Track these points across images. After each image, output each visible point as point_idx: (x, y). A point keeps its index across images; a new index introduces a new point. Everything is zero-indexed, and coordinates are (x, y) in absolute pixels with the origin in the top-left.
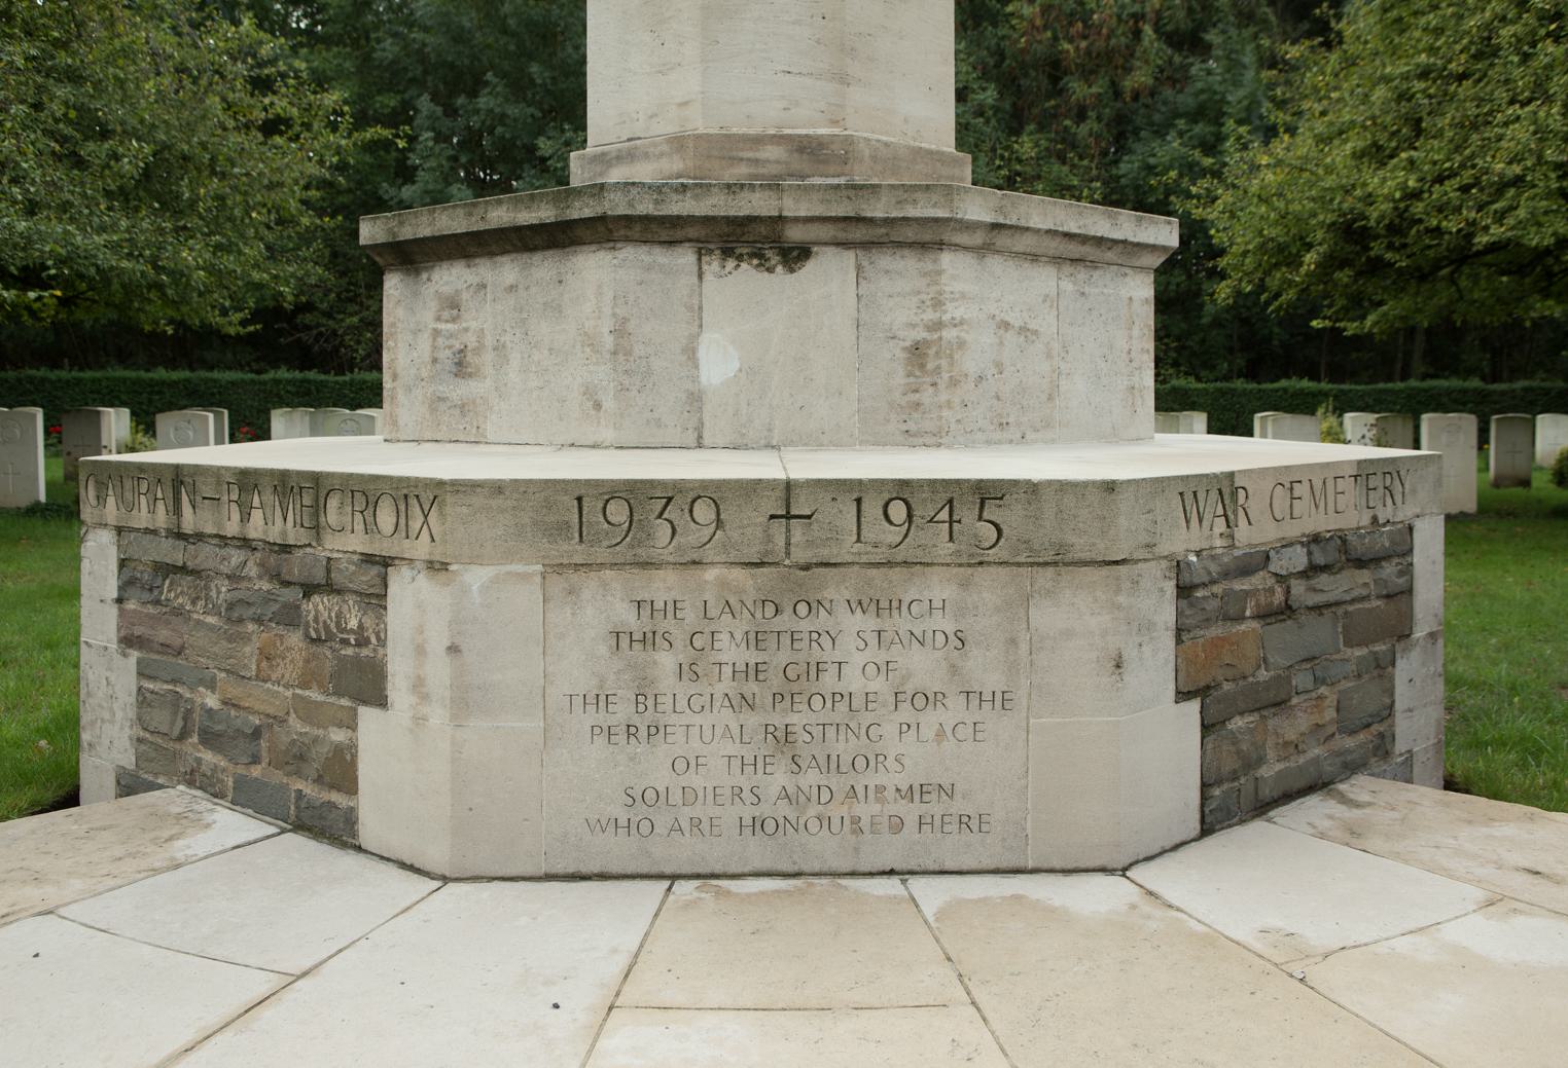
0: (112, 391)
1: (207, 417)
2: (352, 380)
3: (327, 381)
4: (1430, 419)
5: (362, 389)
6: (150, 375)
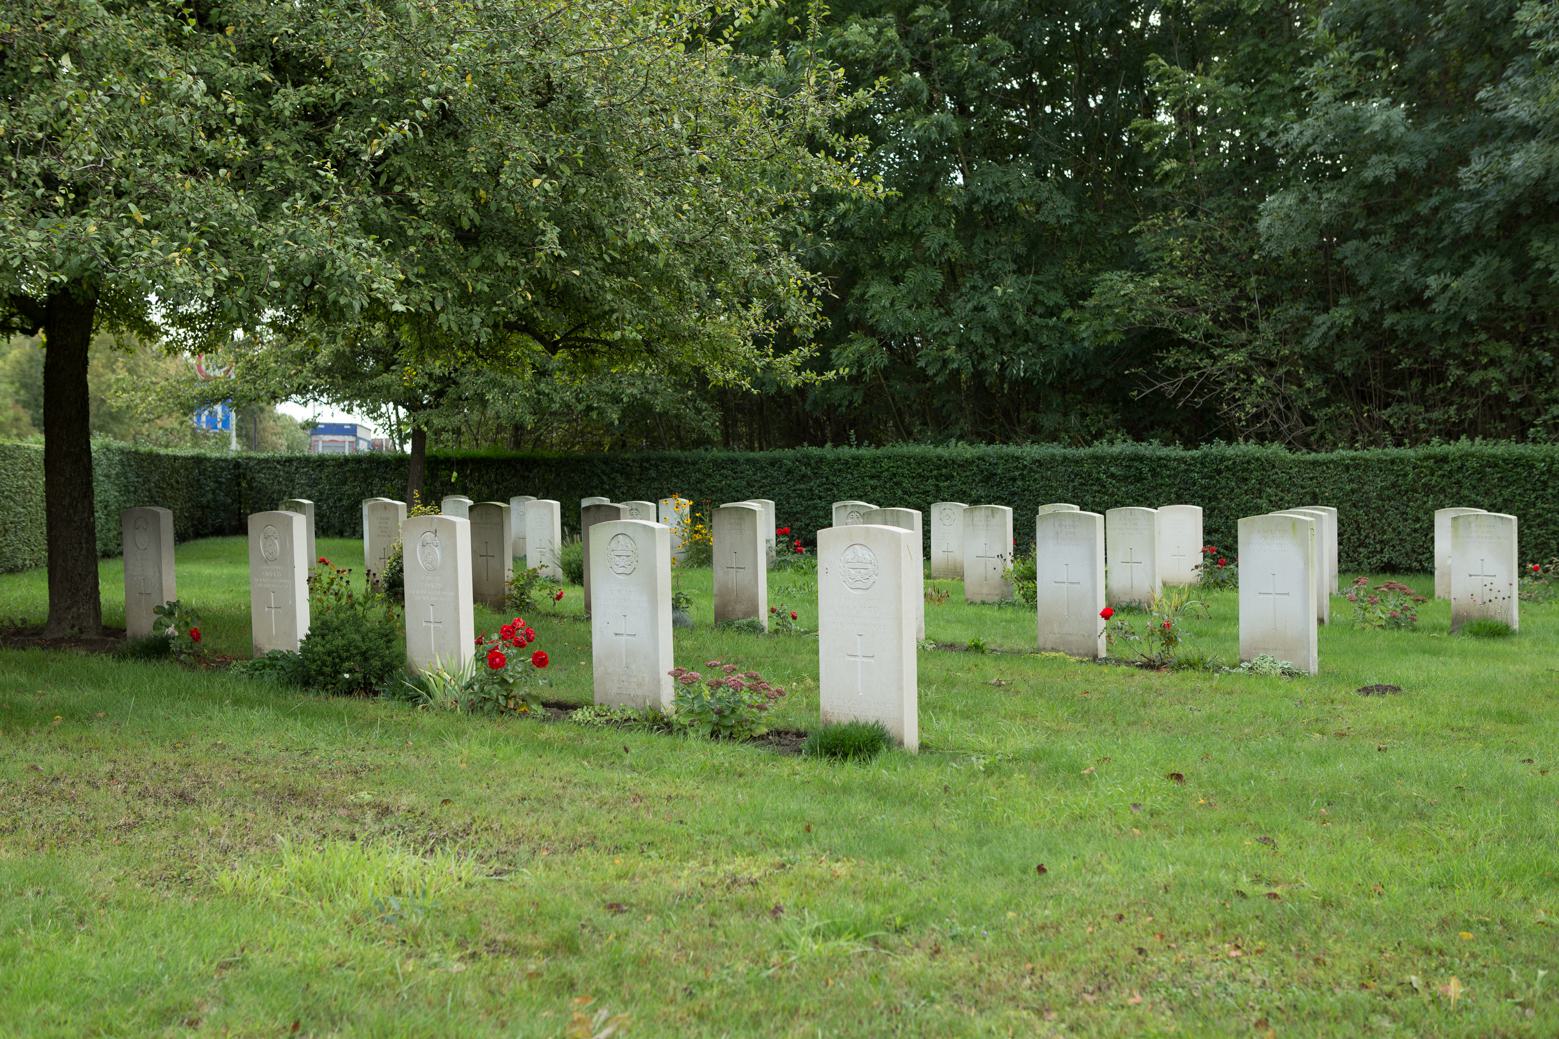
0: (894, 475)
1: (157, 515)
2: (1205, 456)
3: (1168, 459)
4: (372, 509)
5: (1219, 472)
6: (940, 450)
